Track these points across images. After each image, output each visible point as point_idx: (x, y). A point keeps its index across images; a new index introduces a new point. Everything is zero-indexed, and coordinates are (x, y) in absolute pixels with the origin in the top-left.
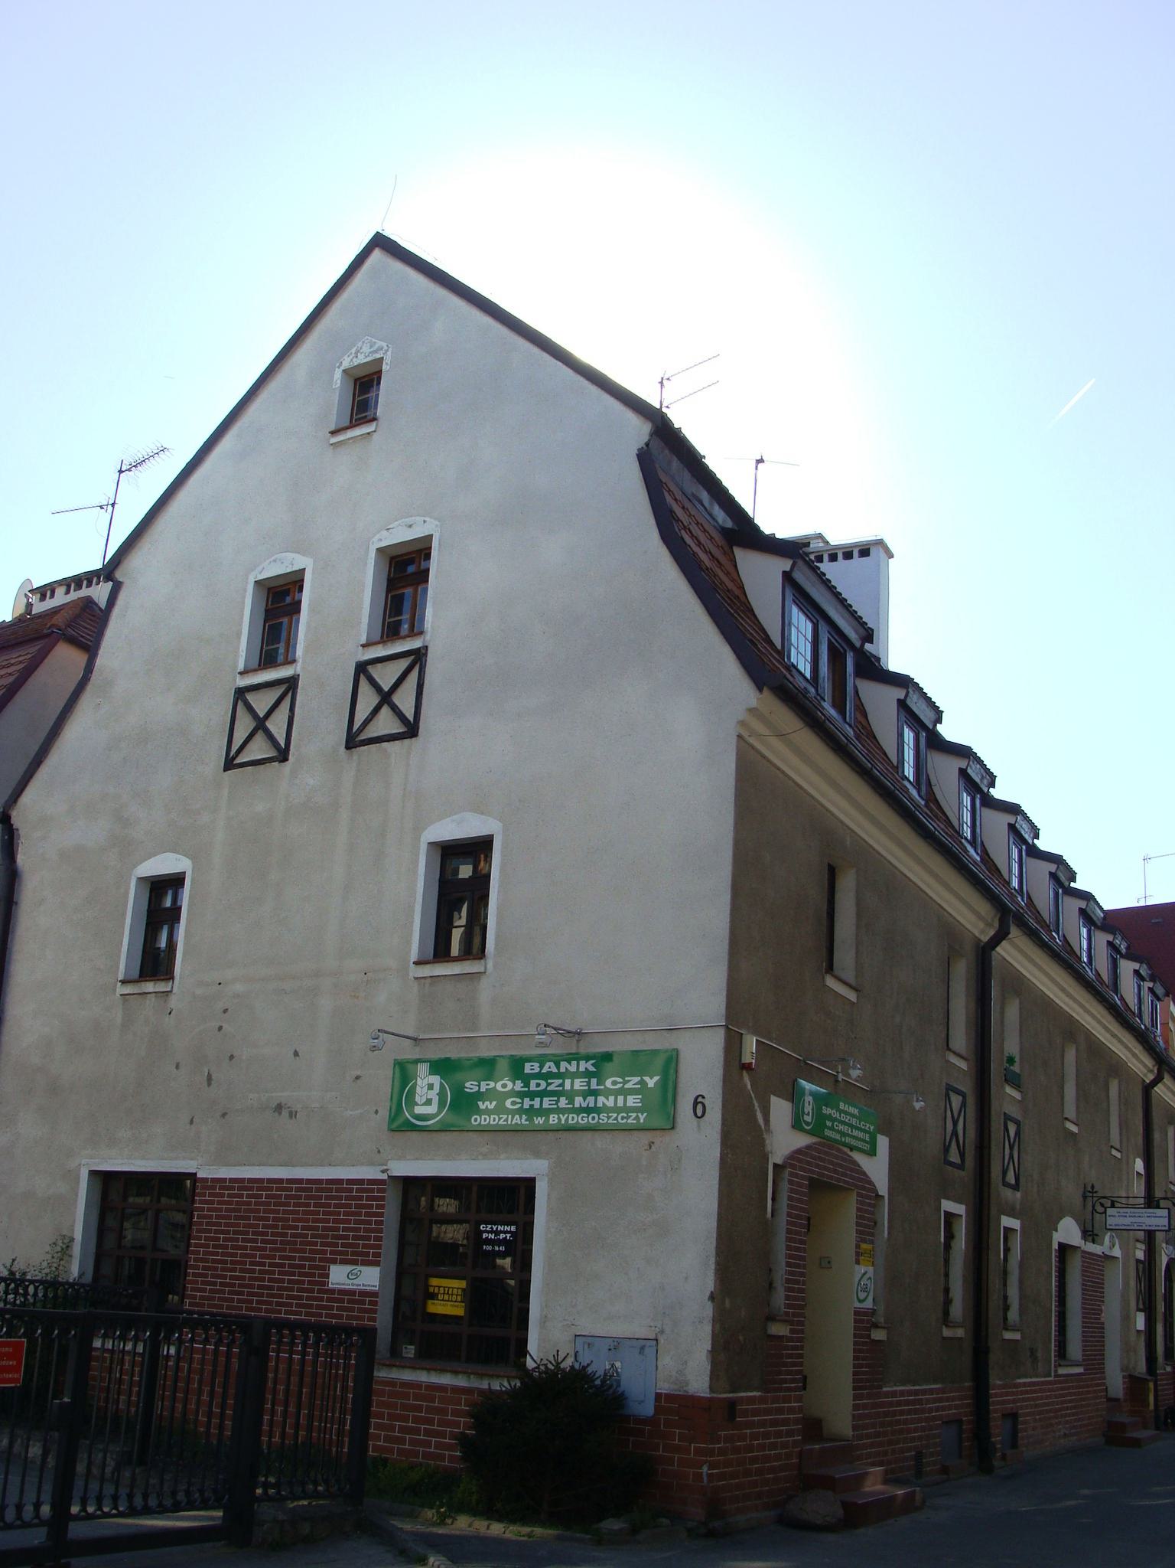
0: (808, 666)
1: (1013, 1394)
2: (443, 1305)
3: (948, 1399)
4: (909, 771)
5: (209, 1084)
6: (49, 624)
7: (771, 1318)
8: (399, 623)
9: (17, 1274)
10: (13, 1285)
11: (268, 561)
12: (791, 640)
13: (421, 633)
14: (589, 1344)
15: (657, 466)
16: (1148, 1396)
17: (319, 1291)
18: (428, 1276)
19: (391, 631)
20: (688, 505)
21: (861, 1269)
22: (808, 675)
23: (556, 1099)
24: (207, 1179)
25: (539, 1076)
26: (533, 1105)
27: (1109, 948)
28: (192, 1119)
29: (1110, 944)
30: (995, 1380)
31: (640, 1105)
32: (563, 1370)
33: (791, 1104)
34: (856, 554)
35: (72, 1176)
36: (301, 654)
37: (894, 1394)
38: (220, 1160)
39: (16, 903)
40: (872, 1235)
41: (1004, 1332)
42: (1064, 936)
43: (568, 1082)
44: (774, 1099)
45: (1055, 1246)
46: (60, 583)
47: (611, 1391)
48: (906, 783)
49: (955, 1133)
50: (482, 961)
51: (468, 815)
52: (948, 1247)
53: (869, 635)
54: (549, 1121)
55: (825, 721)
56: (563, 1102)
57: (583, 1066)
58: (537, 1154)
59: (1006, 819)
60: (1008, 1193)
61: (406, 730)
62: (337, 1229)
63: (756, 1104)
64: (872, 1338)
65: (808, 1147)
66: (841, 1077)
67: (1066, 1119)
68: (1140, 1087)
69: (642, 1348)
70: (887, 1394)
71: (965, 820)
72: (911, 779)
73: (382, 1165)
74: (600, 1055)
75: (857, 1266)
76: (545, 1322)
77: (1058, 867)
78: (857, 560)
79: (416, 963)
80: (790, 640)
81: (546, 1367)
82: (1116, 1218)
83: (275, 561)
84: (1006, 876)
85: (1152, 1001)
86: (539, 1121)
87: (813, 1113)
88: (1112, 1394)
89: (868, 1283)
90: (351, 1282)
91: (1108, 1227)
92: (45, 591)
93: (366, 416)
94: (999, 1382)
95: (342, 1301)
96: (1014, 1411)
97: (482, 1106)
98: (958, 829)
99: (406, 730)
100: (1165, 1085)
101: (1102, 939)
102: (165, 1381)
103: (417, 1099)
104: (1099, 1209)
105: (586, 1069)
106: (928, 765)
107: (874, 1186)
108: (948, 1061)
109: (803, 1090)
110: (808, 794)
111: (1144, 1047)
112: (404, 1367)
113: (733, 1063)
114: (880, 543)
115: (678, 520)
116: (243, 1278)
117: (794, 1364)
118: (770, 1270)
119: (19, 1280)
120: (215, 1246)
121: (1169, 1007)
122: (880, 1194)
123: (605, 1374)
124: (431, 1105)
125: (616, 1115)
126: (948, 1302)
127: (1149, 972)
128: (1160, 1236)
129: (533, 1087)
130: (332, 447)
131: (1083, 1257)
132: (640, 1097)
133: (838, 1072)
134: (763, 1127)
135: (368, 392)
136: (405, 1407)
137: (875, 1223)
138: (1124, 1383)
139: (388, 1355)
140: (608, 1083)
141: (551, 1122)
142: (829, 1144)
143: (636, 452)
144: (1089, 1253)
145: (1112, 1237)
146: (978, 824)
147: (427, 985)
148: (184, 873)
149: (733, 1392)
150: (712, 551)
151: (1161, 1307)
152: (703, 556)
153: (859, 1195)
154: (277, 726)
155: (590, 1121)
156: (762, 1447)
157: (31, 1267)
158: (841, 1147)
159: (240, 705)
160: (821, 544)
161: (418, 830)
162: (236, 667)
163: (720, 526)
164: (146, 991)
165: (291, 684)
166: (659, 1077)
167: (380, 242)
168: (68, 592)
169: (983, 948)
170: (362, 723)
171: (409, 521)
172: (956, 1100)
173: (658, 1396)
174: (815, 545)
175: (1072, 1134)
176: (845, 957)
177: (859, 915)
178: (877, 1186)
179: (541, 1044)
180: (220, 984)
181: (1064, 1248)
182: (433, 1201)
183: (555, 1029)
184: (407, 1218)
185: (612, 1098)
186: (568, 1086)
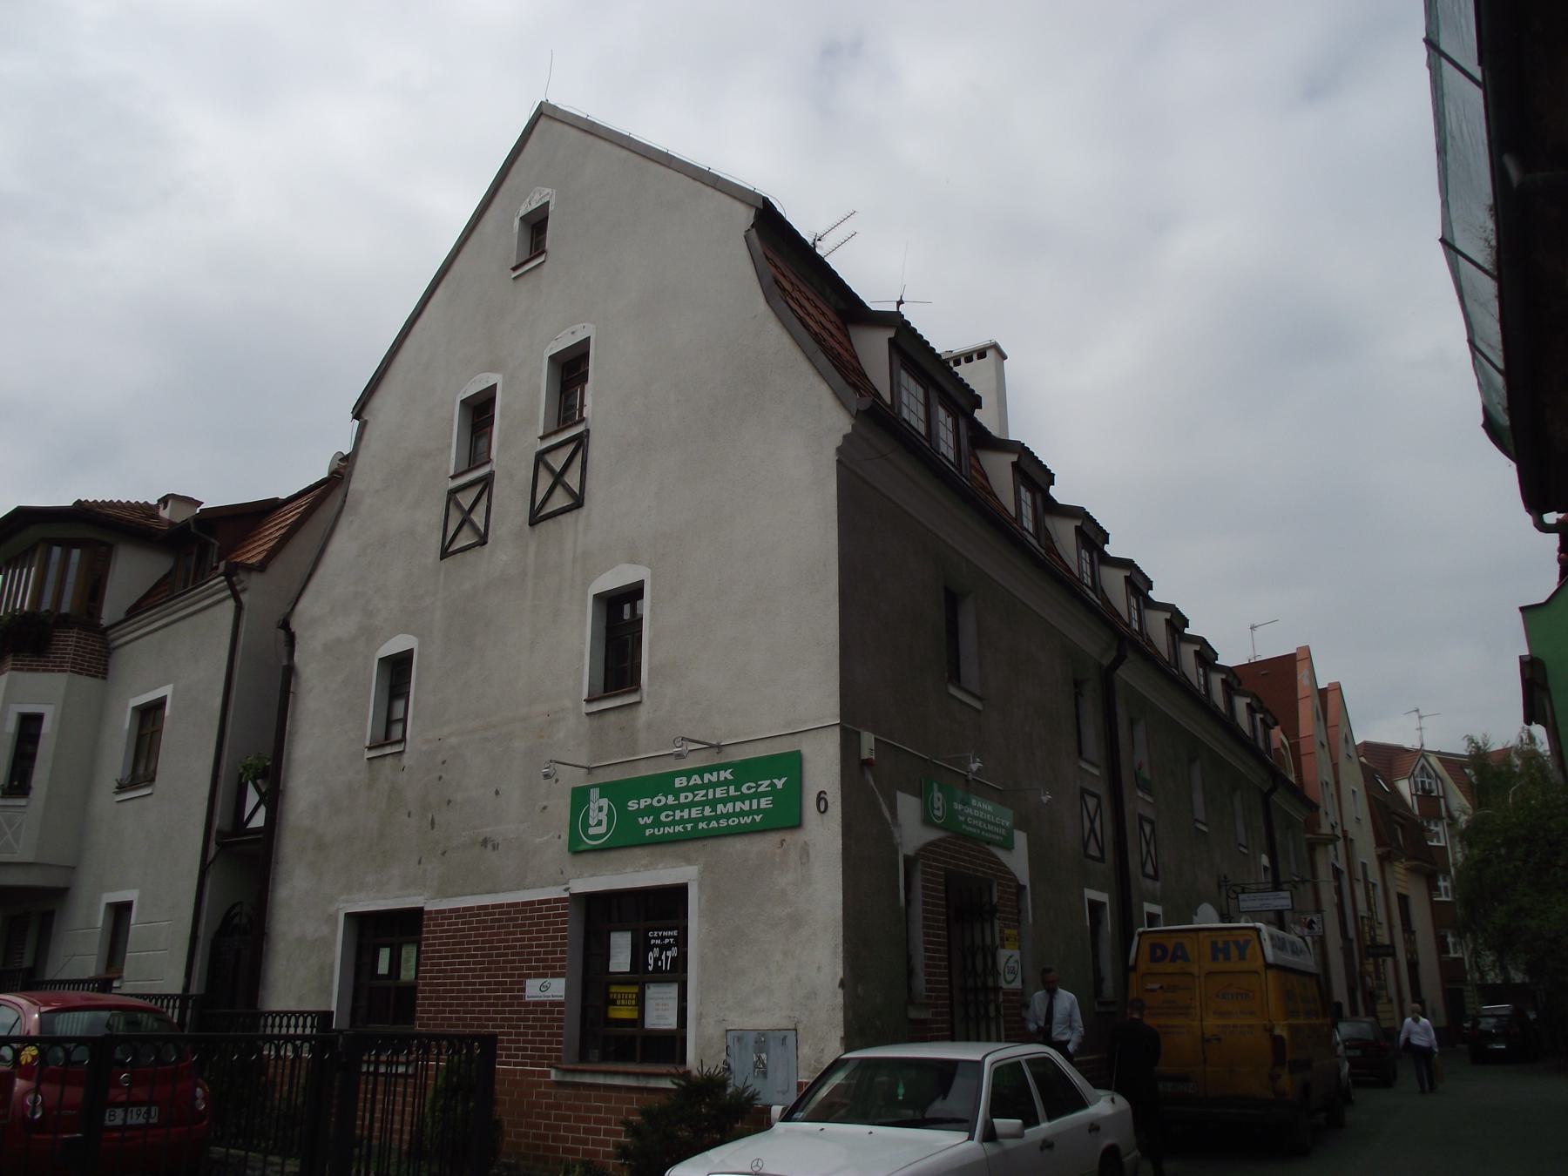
5: (433, 828)
23: (700, 808)
31: (771, 806)
35: (332, 919)
38: (442, 893)
43: (711, 791)
49: (1092, 830)
51: (624, 567)
56: (707, 811)
58: (689, 861)
63: (881, 799)
65: (940, 840)
69: (784, 1039)
71: (1088, 566)
72: (1031, 530)
73: (565, 884)
76: (700, 1019)
78: (976, 362)
79: (588, 701)
82: (1247, 902)
90: (542, 994)
91: (1241, 910)
102: (405, 1091)
107: (1014, 875)
108: (1080, 767)
113: (852, 765)
122: (1021, 883)
129: (682, 800)
132: (771, 798)
140: (744, 789)
154: (478, 518)
161: (586, 584)
162: (448, 472)
167: (544, 113)
172: (1091, 803)
176: (969, 669)
185: (747, 802)
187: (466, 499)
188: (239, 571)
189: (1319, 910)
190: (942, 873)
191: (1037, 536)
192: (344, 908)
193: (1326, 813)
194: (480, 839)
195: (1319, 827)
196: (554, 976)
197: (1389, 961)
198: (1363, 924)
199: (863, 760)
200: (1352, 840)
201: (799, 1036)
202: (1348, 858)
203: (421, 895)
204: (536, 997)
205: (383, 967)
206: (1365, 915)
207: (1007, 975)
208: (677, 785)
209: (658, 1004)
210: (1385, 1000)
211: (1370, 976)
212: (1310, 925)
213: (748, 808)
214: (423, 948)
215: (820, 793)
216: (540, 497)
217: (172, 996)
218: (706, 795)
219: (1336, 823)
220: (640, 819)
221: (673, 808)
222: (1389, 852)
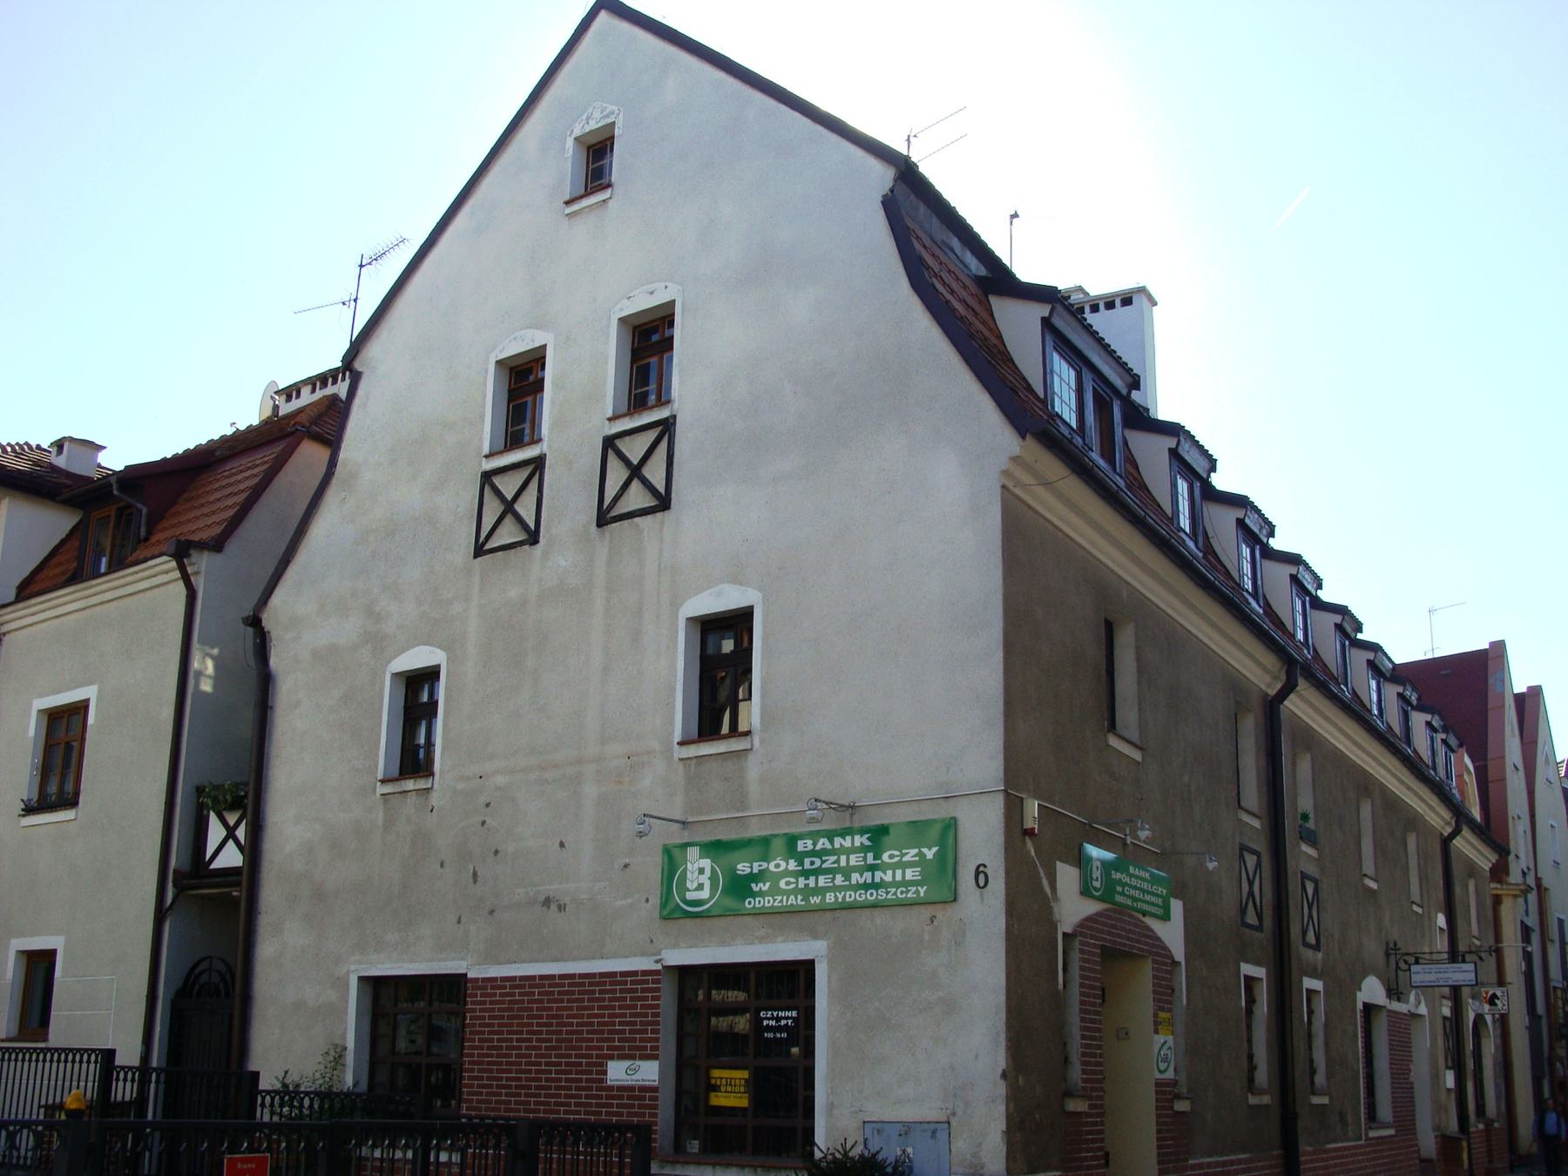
0: (1074, 416)
2: (726, 1097)
4: (1185, 523)
5: (475, 881)
6: (293, 423)
7: (1068, 1094)
8: (646, 395)
9: (291, 1086)
10: (287, 1098)
11: (509, 339)
12: (1053, 388)
13: (668, 402)
14: (878, 1130)
15: (904, 213)
16: (1462, 1154)
18: (708, 1069)
19: (638, 403)
20: (937, 252)
21: (1159, 1039)
22: (1074, 424)
23: (831, 876)
26: (808, 884)
27: (1400, 700)
28: (460, 918)
30: (1305, 1147)
32: (852, 1159)
33: (1078, 870)
34: (1118, 303)
36: (546, 434)
38: (490, 958)
39: (271, 708)
40: (1170, 1003)
42: (1353, 690)
43: (843, 858)
44: (1059, 865)
45: (1360, 1006)
49: (1251, 893)
50: (748, 738)
51: (726, 587)
52: (1249, 1012)
53: (1135, 383)
54: (825, 900)
55: (1092, 467)
56: (839, 880)
57: (858, 840)
58: (815, 936)
60: (1309, 954)
61: (658, 503)
62: (613, 1024)
63: (1041, 872)
64: (1175, 1109)
65: (1098, 914)
66: (1129, 840)
67: (1365, 875)
68: (1439, 840)
69: (934, 1132)
72: (1187, 530)
74: (875, 828)
76: (831, 1110)
77: (1343, 619)
78: (1119, 310)
79: (681, 744)
81: (835, 1158)
82: (1420, 974)
83: (515, 339)
84: (1290, 629)
85: (1446, 753)
86: (815, 900)
87: (1102, 876)
88: (1424, 1154)
90: (629, 1077)
91: (1413, 984)
92: (290, 392)
93: (601, 184)
94: (1308, 1149)
95: (621, 1098)
98: (1238, 581)
99: (658, 503)
100: (1464, 838)
101: (1391, 691)
103: (689, 885)
104: (1403, 966)
105: (861, 843)
106: (1204, 515)
107: (1170, 951)
109: (1090, 859)
110: (1080, 546)
112: (688, 1163)
114: (1142, 290)
115: (928, 268)
117: (1094, 1141)
118: (1065, 1044)
119: (292, 1092)
121: (1463, 759)
122: (1176, 959)
123: (897, 1161)
124: (702, 889)
125: (895, 889)
126: (1252, 1069)
127: (1442, 723)
128: (1465, 992)
129: (807, 865)
130: (567, 218)
131: (1388, 1016)
132: (919, 869)
133: (1126, 835)
134: (1050, 895)
135: (602, 160)
137: (1173, 991)
140: (885, 857)
141: (828, 901)
142: (1122, 910)
143: (880, 199)
144: (1395, 1012)
145: (1417, 994)
147: (693, 767)
148: (438, 666)
150: (966, 300)
151: (1470, 1064)
152: (957, 305)
153: (1154, 962)
154: (526, 508)
155: (868, 896)
157: (304, 1079)
158: (1134, 913)
159: (487, 489)
160: (1082, 296)
161: (675, 605)
162: (480, 447)
163: (975, 276)
164: (406, 789)
165: (538, 464)
166: (937, 848)
168: (313, 391)
169: (1271, 701)
170: (612, 500)
171: (650, 287)
172: (1251, 860)
174: (1075, 298)
176: (1127, 714)
177: (1140, 671)
178: (1172, 951)
179: (812, 820)
180: (481, 777)
181: (1369, 1009)
182: (710, 994)
183: (827, 803)
184: (685, 1009)
185: (889, 873)
186: (843, 863)
187: (508, 485)
188: (192, 552)
189: (1501, 982)
190: (1098, 951)
192: (357, 970)
194: (542, 898)
195: (1508, 874)
198: (1556, 998)
199: (1026, 830)
200: (1546, 889)
203: (462, 959)
204: (621, 1081)
206: (1561, 986)
211: (1563, 1064)
212: (1492, 1000)
214: (468, 1021)
215: (978, 867)
216: (610, 493)
217: (130, 1068)
219: (1528, 868)
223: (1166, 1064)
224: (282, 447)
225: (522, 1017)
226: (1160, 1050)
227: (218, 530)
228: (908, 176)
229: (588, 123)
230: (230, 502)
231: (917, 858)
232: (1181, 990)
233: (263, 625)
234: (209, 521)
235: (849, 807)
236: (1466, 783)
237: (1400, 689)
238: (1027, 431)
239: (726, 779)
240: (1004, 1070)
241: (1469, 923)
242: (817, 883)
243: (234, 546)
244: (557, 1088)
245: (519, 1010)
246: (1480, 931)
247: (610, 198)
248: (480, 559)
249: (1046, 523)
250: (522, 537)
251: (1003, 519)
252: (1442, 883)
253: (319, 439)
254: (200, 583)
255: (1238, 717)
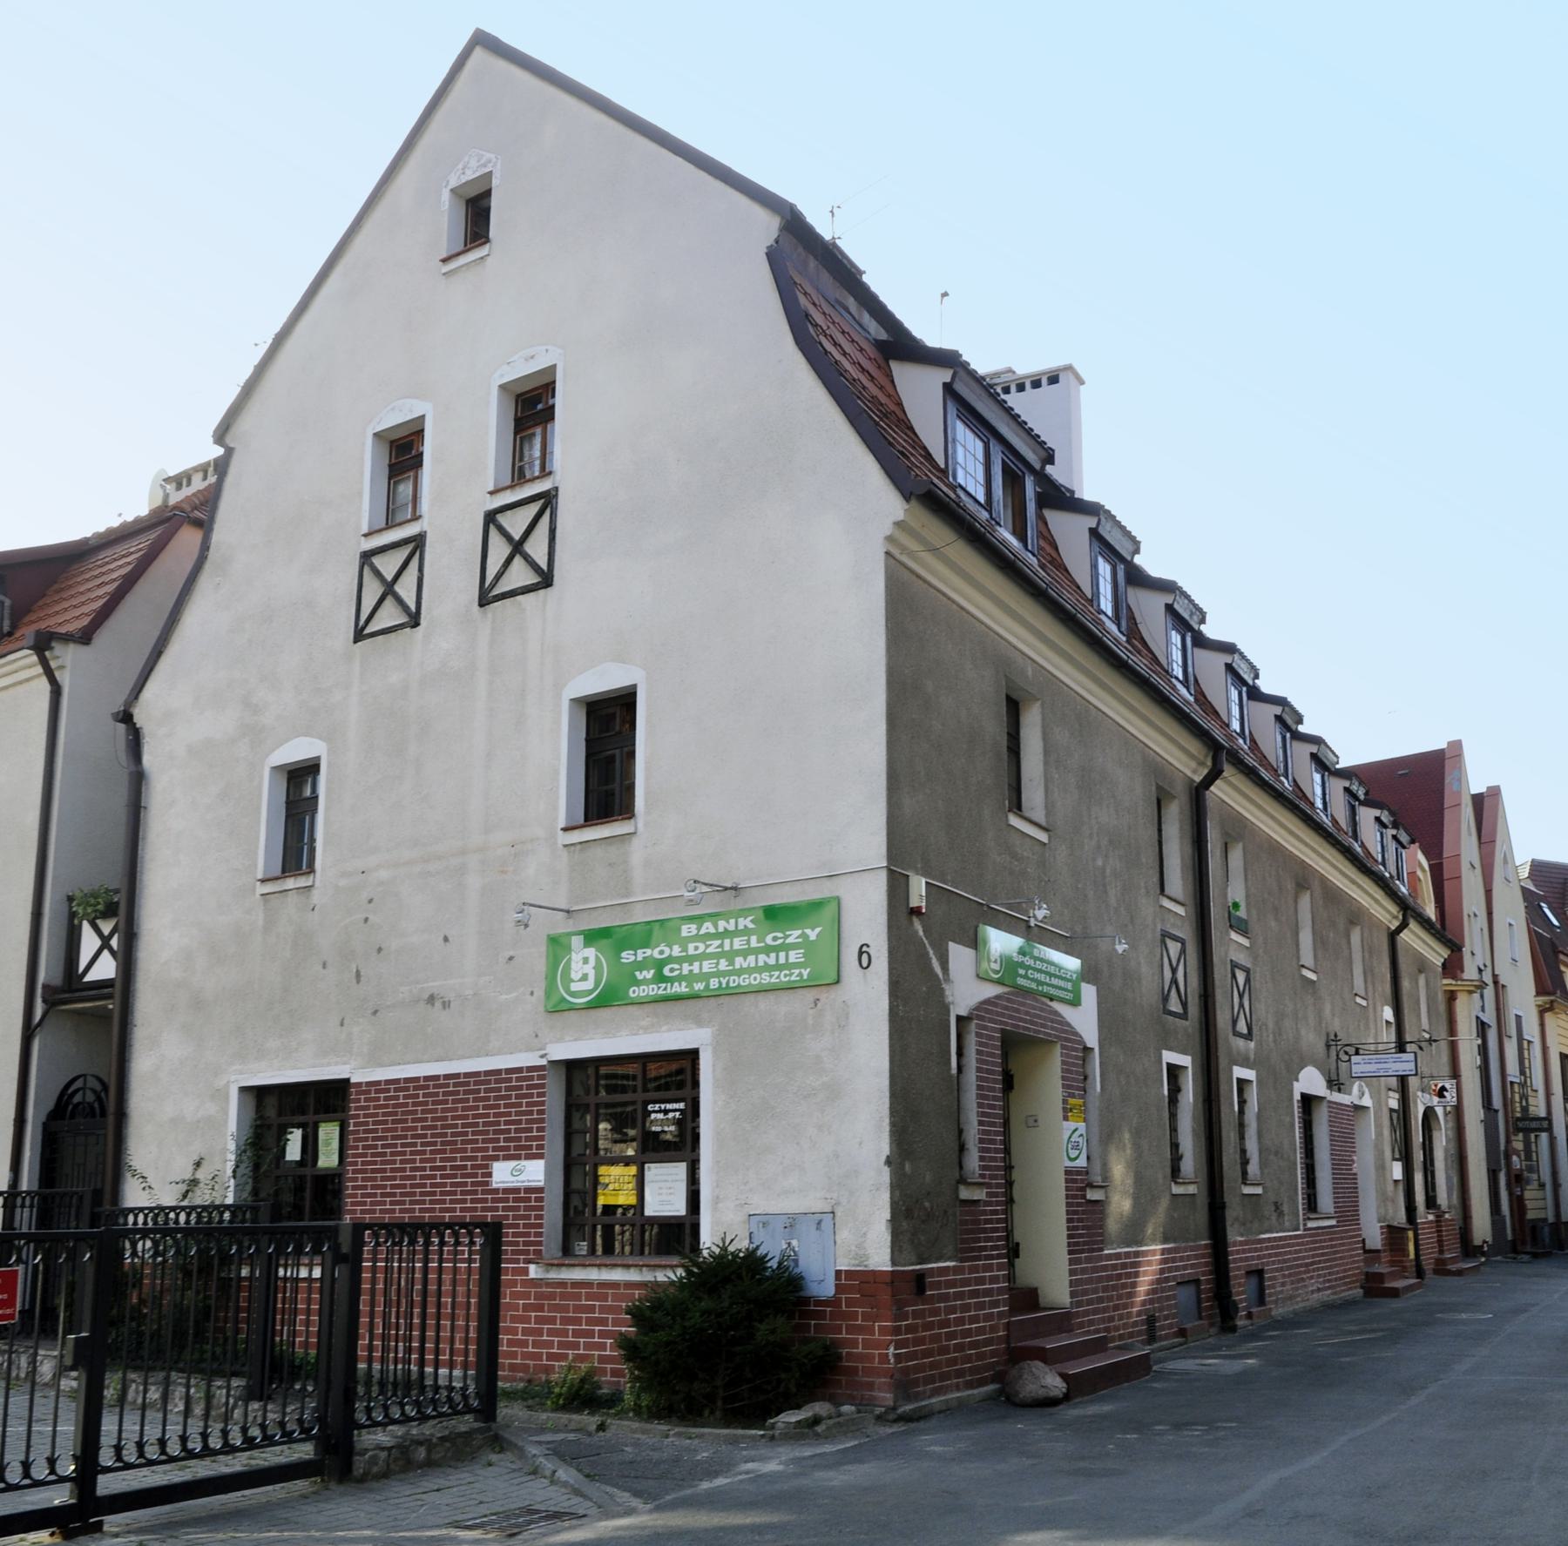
1: (1256, 1250)
3: (1182, 1259)
4: (1106, 605)
5: (358, 982)
7: (962, 1181)
16: (1407, 1245)
17: (483, 1192)
19: (519, 476)
21: (1070, 1125)
24: (361, 1083)
25: (698, 938)
28: (343, 1019)
29: (1347, 790)
30: (1234, 1236)
34: (1044, 381)
37: (1118, 1256)
38: (374, 1061)
39: (145, 808)
41: (1243, 1186)
42: (1295, 781)
43: (727, 942)
44: (952, 946)
45: (1297, 1097)
46: (196, 469)
47: (786, 1274)
48: (1102, 617)
49: (1174, 981)
50: (632, 821)
58: (699, 1023)
59: (1162, 599)
61: (540, 580)
62: (498, 1123)
63: (931, 952)
65: (997, 997)
67: (1303, 966)
69: (819, 1223)
70: (1109, 1257)
71: (1174, 658)
73: (541, 1049)
75: (1065, 1123)
77: (1283, 710)
78: (1045, 388)
80: (954, 458)
82: (1360, 1065)
85: (1397, 849)
86: (699, 986)
88: (1370, 1245)
89: (1080, 1140)
92: (180, 480)
95: (507, 1200)
96: (1260, 1267)
97: (639, 976)
99: (540, 580)
101: (1337, 785)
107: (1081, 1037)
108: (1161, 906)
111: (1386, 893)
113: (900, 911)
114: (1069, 368)
116: (404, 1186)
120: (373, 1155)
121: (1416, 854)
122: (1089, 1046)
127: (1392, 819)
129: (691, 951)
132: (802, 951)
134: (941, 976)
136: (578, 1309)
138: (1382, 1233)
139: (560, 1254)
140: (769, 940)
143: (765, 250)
145: (1360, 1086)
146: (1190, 662)
148: (318, 758)
149: (920, 1264)
151: (1418, 1156)
152: (847, 365)
153: (1063, 1047)
154: (406, 589)
156: (960, 1321)
159: (366, 570)
163: (875, 340)
165: (418, 542)
168: (205, 478)
171: (529, 352)
172: (1174, 948)
173: (838, 1273)
175: (1313, 982)
176: (1034, 795)
181: (1308, 1101)
188: (54, 644)
189: (1455, 1074)
191: (1117, 619)
192: (237, 1081)
193: (1473, 954)
194: (426, 996)
195: (1462, 971)
196: (530, 1157)
197: (1544, 1136)
198: (1513, 1092)
199: (912, 908)
200: (1503, 986)
201: (837, 1219)
202: (1498, 1009)
203: (345, 1064)
205: (293, 1151)
207: (1070, 1151)
208: (684, 933)
209: (661, 1188)
210: (1535, 1185)
211: (1519, 1156)
213: (774, 963)
215: (862, 946)
218: (721, 946)
219: (1485, 966)
220: (637, 973)
221: (680, 960)
222: (1552, 1002)
223: (1078, 1152)
224: (157, 533)
225: (406, 1121)
226: (1070, 1137)
227: (85, 621)
228: (795, 227)
229: (464, 173)
230: (101, 592)
231: (800, 940)
232: (1095, 1076)
233: (135, 721)
234: (77, 612)
235: (731, 888)
236: (1420, 880)
237: (1347, 784)
238: (911, 494)
239: (610, 864)
240: (888, 1157)
241: (1419, 1016)
242: (701, 968)
243: (103, 637)
244: (442, 1193)
245: (404, 1113)
246: (1430, 1024)
247: (488, 255)
248: (360, 643)
249: (938, 594)
250: (403, 619)
251: (887, 587)
252: (1389, 976)
253: (198, 524)
254: (64, 678)
255: (1162, 803)
